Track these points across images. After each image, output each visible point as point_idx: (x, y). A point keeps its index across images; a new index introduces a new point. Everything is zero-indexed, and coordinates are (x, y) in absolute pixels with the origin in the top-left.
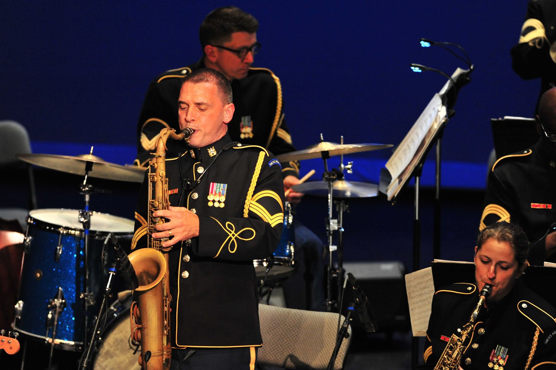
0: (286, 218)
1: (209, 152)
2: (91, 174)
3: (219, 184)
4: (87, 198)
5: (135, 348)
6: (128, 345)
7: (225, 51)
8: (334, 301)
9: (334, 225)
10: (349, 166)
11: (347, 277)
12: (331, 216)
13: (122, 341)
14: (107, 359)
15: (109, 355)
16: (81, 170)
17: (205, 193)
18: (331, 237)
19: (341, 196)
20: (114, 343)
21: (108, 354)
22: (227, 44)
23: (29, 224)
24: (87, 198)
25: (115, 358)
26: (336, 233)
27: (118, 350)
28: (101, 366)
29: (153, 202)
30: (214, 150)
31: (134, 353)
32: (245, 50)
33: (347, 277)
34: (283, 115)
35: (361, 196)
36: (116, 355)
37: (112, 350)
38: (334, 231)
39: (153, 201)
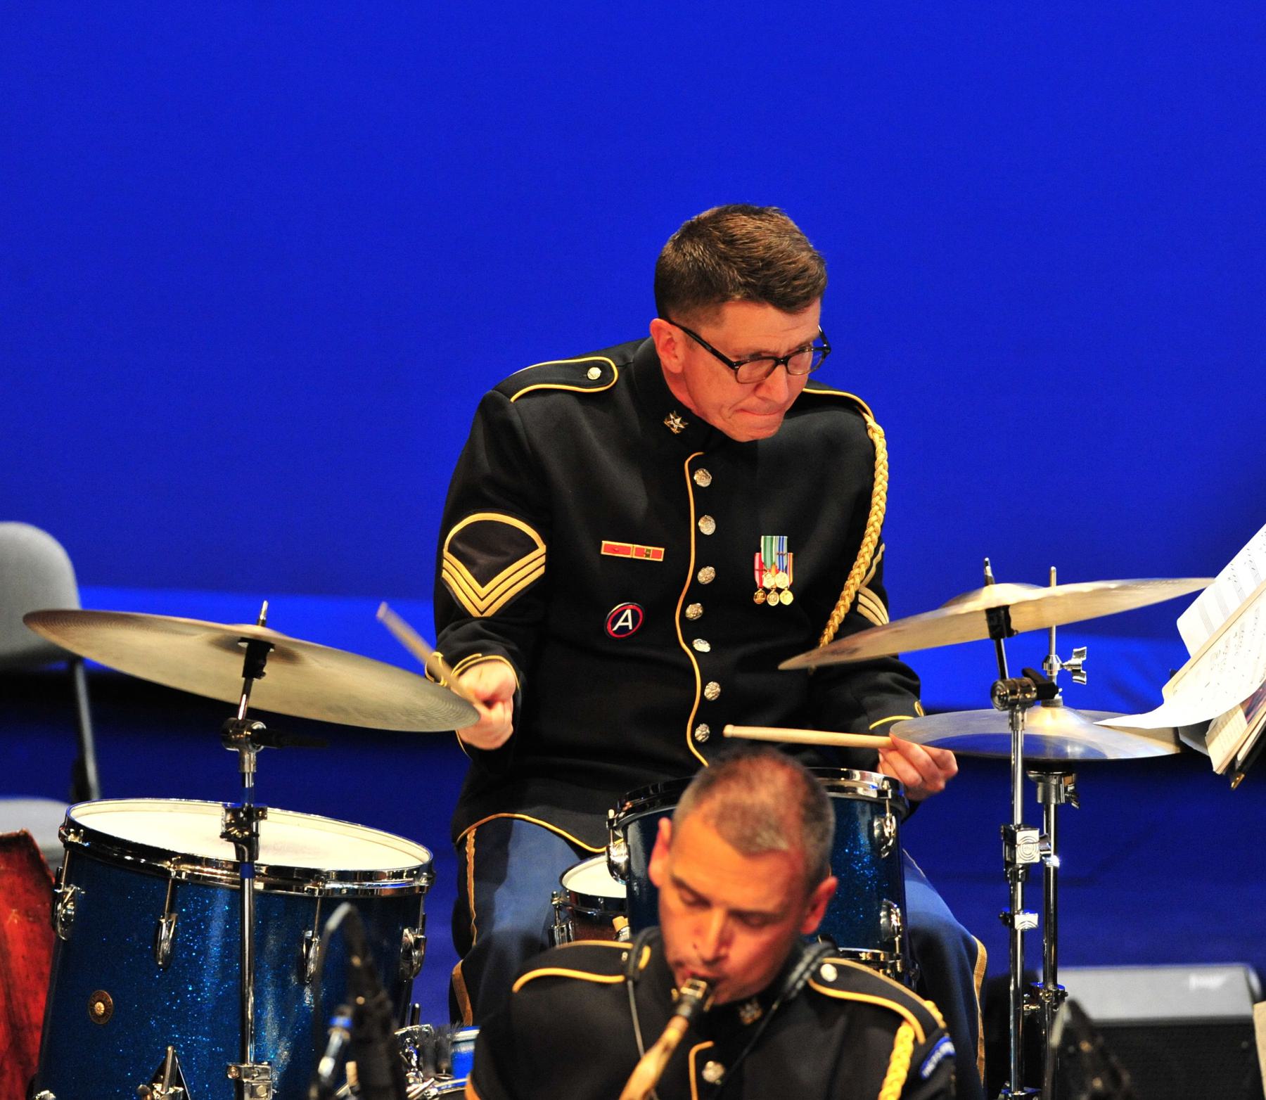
0: (876, 824)
4: (249, 762)
7: (701, 348)
8: (1029, 1090)
9: (1029, 847)
10: (1076, 661)
11: (1064, 1014)
12: (1018, 819)
18: (1019, 884)
19: (1050, 755)
22: (707, 332)
23: (68, 845)
24: (249, 762)
26: (1036, 871)
32: (770, 363)
34: (883, 547)
35: (1111, 756)
38: (1027, 867)
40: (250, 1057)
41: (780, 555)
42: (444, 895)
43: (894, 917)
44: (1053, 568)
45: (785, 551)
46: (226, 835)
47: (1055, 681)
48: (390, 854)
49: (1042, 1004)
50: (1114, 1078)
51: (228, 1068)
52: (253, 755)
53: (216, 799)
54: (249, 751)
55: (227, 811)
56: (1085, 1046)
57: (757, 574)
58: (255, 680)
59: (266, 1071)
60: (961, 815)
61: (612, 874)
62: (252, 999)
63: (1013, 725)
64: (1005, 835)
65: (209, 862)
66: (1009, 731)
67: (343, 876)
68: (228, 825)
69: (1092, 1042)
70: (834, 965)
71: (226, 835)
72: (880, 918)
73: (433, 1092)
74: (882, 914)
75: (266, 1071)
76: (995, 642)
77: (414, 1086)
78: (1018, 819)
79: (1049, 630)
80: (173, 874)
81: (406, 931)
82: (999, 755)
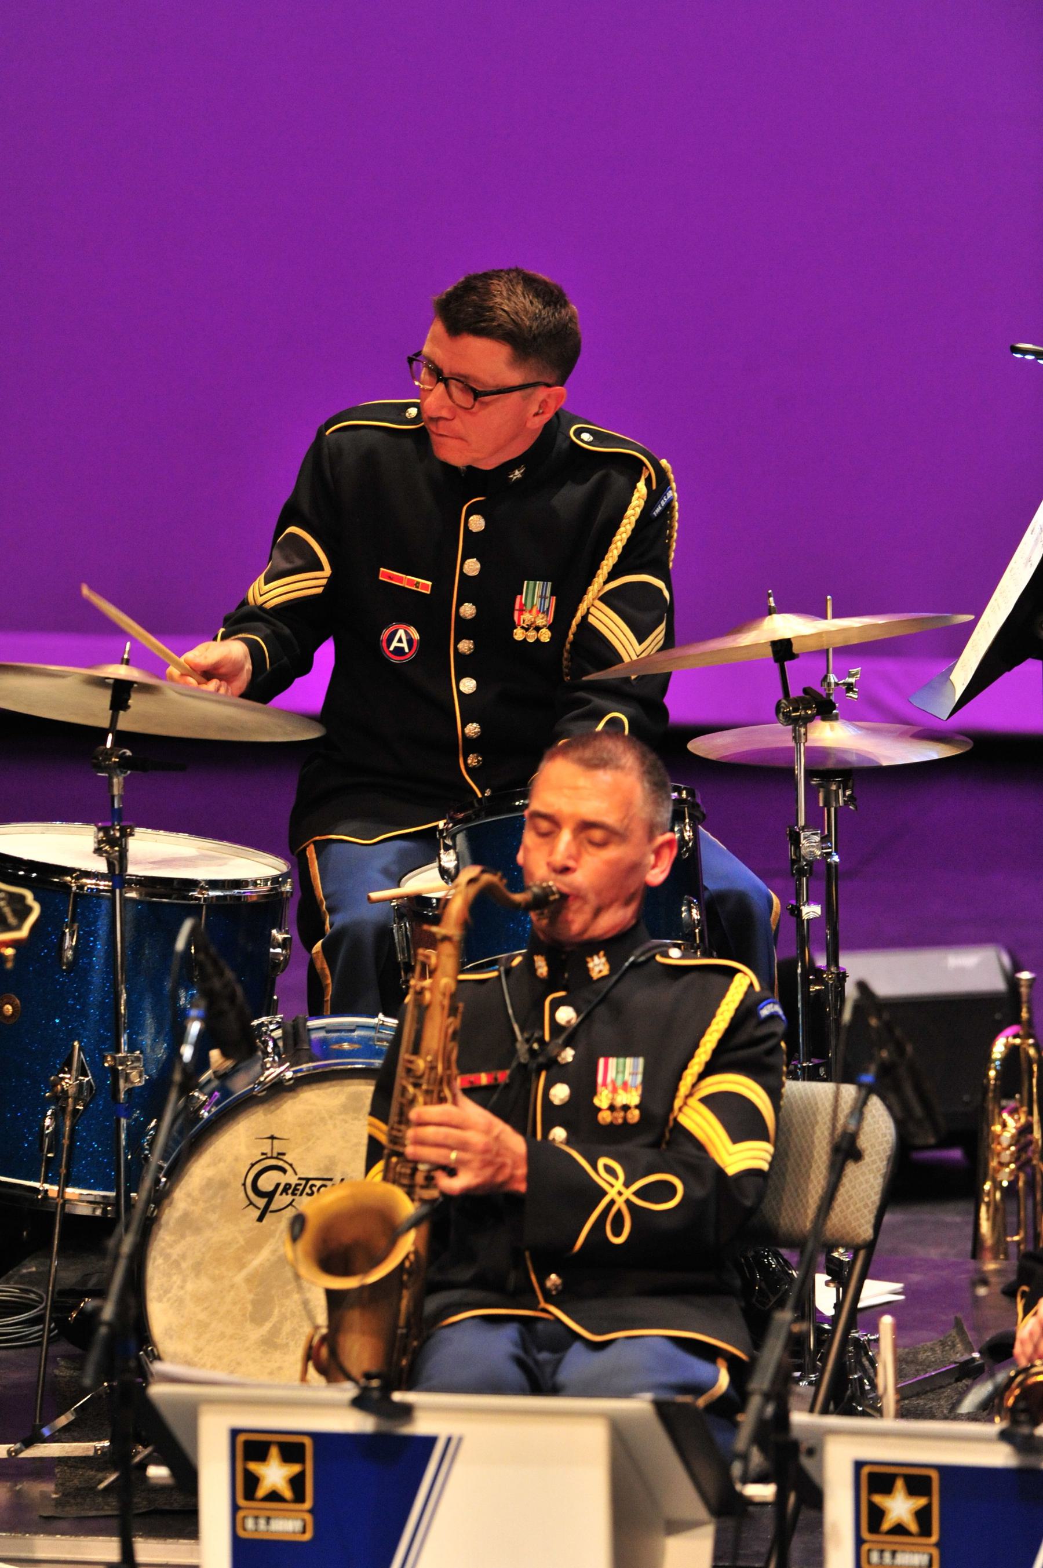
1: (591, 965)
2: (125, 723)
3: (621, 1060)
5: (261, 1202)
6: (242, 1194)
8: (816, 1061)
9: (811, 844)
12: (802, 822)
13: (224, 1185)
14: (183, 1236)
15: (187, 1222)
16: (92, 709)
17: (585, 1083)
19: (830, 764)
20: (202, 1191)
21: (187, 1222)
25: (208, 1233)
27: (214, 1211)
28: (167, 1257)
29: (411, 1062)
30: (603, 960)
31: (260, 1219)
33: (850, 991)
36: (210, 1225)
37: (197, 1210)
39: (413, 1058)
40: (124, 1047)
41: (543, 597)
43: (694, 911)
44: (829, 597)
45: (548, 594)
46: (98, 851)
47: (832, 698)
49: (826, 984)
50: (900, 1049)
51: (105, 1057)
52: (121, 778)
53: (86, 820)
54: (118, 776)
55: (100, 829)
56: (874, 1022)
57: (516, 614)
58: (121, 712)
59: (138, 1059)
61: (443, 878)
62: (124, 996)
63: (796, 738)
64: (791, 835)
65: (87, 874)
66: (792, 744)
67: (214, 884)
68: (100, 842)
69: (879, 1017)
70: (670, 958)
71: (98, 851)
72: (681, 912)
73: (289, 1075)
74: (683, 909)
75: (138, 1059)
76: (777, 665)
77: (272, 1070)
78: (802, 822)
79: (828, 650)
80: (74, 889)
81: (274, 932)
82: (783, 765)
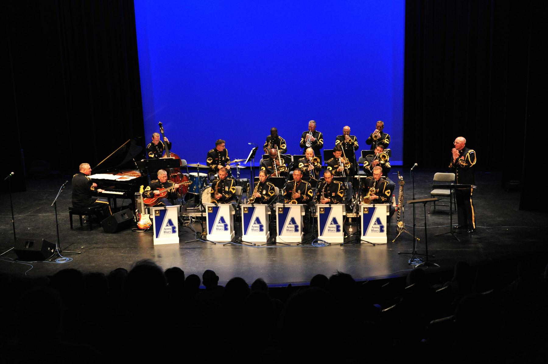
42: (208, 177)
48: (206, 175)
60: (234, 170)
